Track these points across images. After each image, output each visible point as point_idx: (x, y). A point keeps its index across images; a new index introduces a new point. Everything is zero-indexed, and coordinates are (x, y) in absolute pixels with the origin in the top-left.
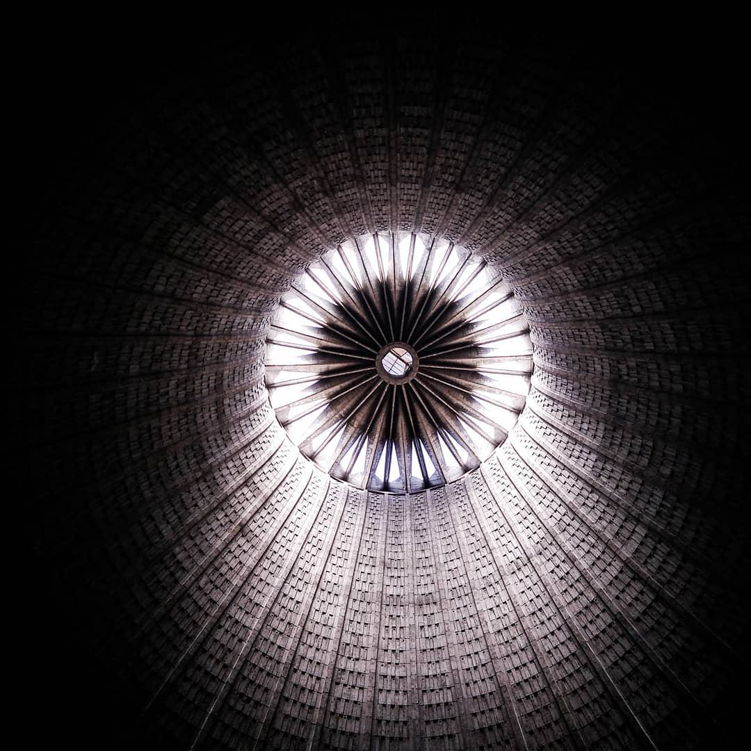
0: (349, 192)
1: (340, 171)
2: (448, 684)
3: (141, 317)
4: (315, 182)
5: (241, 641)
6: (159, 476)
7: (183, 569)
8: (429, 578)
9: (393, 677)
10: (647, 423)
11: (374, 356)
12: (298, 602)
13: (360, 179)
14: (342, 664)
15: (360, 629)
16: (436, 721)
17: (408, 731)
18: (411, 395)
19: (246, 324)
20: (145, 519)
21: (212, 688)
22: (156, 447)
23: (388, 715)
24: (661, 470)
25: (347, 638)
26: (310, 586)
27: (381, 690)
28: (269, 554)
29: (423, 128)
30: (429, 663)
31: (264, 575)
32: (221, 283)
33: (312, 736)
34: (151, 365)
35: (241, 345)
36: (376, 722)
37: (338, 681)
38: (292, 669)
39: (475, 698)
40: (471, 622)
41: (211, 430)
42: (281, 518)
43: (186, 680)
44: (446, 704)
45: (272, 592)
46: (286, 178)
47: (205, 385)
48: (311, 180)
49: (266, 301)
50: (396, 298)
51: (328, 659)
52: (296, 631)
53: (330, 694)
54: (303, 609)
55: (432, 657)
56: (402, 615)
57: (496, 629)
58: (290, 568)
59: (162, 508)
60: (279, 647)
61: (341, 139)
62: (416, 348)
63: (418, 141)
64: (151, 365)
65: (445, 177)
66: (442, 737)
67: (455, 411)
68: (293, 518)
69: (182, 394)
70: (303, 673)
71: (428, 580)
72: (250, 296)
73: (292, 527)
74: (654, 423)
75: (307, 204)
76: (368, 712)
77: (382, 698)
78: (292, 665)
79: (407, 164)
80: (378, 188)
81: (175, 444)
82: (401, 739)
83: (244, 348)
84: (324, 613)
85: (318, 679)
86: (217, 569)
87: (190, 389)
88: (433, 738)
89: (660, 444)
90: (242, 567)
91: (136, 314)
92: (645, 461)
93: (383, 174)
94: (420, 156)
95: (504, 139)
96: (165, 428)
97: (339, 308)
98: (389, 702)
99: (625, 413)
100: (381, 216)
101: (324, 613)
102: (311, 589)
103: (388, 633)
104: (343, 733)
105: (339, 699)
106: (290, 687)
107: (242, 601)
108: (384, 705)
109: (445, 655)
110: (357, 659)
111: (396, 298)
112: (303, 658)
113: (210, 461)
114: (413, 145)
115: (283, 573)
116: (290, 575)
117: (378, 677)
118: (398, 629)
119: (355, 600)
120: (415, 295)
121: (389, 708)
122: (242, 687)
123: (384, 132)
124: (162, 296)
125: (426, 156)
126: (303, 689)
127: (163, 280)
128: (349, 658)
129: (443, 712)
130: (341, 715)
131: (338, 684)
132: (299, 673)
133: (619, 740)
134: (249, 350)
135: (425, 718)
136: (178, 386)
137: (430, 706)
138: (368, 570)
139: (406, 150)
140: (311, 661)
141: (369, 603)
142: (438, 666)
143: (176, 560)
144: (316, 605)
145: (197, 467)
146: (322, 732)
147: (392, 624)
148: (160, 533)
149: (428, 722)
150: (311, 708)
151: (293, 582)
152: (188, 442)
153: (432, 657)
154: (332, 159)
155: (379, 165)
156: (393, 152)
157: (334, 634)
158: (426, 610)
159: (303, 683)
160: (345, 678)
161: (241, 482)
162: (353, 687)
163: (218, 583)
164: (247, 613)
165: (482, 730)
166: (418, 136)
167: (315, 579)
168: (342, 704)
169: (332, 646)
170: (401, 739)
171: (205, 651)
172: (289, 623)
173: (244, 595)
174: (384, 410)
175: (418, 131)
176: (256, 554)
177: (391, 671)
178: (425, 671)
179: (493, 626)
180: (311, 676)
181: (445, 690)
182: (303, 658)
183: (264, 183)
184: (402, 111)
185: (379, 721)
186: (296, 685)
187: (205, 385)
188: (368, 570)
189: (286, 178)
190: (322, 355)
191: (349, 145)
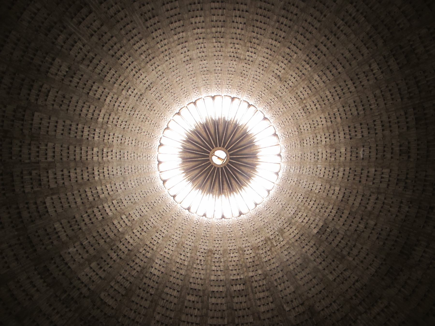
0: (258, 240)
1: (265, 251)
2: (173, 31)
4: (275, 245)
8: (189, 70)
10: (108, 167)
11: (230, 155)
13: (256, 248)
16: (176, 15)
18: (210, 144)
19: (293, 169)
20: (327, 82)
24: (98, 149)
29: (233, 280)
30: (183, 38)
32: (309, 190)
35: (294, 159)
39: (159, 29)
41: (302, 121)
44: (172, 23)
46: (289, 246)
47: (308, 142)
48: (277, 245)
49: (286, 180)
55: (181, 40)
56: (199, 54)
57: (155, 59)
59: (320, 87)
60: (254, 32)
61: (268, 268)
62: (212, 166)
63: (234, 272)
65: (218, 256)
66: (171, 9)
71: (188, 70)
72: (294, 184)
74: (105, 168)
75: (276, 232)
77: (202, 19)
79: (236, 259)
80: (246, 244)
82: (190, 4)
83: (292, 158)
87: (315, 141)
88: (175, 8)
89: (100, 160)
91: (346, 176)
92: (105, 150)
93: (245, 252)
94: (231, 264)
95: (198, 282)
96: (324, 122)
98: (199, 18)
99: (118, 168)
100: (241, 229)
103: (204, 45)
109: (177, 42)
113: (300, 107)
114: (236, 270)
118: (199, 48)
120: (217, 189)
123: (251, 274)
125: (229, 265)
127: (336, 193)
129: (173, 20)
133: (92, 30)
134: (290, 156)
135: (181, 15)
137: (179, 21)
138: (217, 68)
139: (238, 267)
142: (179, 37)
143: (309, 65)
145: (306, 105)
147: (203, 50)
149: (179, 14)
152: (312, 116)
153: (181, 40)
154: (270, 257)
155: (248, 257)
156: (244, 265)
158: (188, 58)
165: (154, 17)
166: (234, 275)
175: (235, 278)
177: (199, 31)
178: (184, 34)
179: (156, 60)
181: (173, 28)
183: (298, 242)
184: (244, 286)
187: (308, 142)
188: (217, 68)
189: (289, 246)
191: (264, 265)
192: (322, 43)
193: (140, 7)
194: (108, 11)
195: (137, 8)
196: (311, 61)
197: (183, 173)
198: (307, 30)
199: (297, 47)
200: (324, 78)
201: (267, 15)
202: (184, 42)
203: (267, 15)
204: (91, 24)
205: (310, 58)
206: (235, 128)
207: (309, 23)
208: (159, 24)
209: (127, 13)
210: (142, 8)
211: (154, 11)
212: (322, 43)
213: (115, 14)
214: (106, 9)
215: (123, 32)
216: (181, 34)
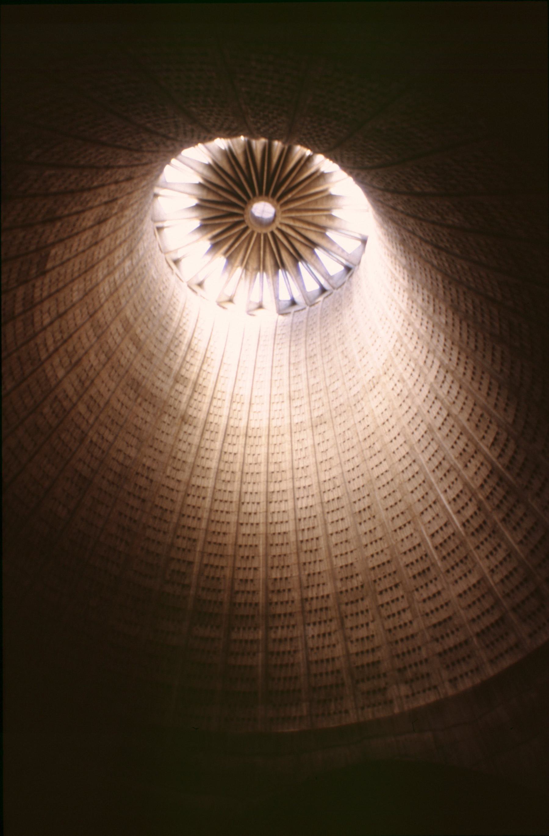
3: (46, 345)
5: (204, 498)
6: (113, 420)
7: (153, 470)
9: (304, 487)
12: (235, 454)
14: (271, 488)
15: (279, 458)
17: (317, 521)
21: (195, 535)
22: (102, 405)
23: (304, 514)
25: (272, 468)
26: (241, 437)
27: (298, 499)
28: (208, 427)
30: (325, 471)
31: (207, 446)
33: (261, 542)
34: (71, 362)
36: (298, 521)
37: (271, 501)
38: (241, 503)
40: (348, 434)
42: (209, 392)
43: (178, 537)
45: (216, 455)
50: (241, 159)
51: (261, 488)
52: (238, 476)
53: (267, 512)
54: (239, 458)
58: (224, 431)
62: (273, 195)
64: (71, 362)
67: (322, 229)
68: (219, 387)
69: (103, 357)
70: (248, 503)
73: (219, 396)
76: (292, 516)
77: (299, 504)
78: (240, 500)
81: (114, 392)
84: (254, 455)
85: (258, 503)
86: (175, 458)
87: (106, 349)
90: (191, 447)
91: (41, 347)
97: (209, 166)
101: (254, 455)
102: (242, 440)
104: (279, 534)
105: (273, 513)
106: (242, 515)
107: (198, 471)
108: (301, 508)
110: (281, 481)
111: (241, 159)
112: (246, 493)
115: (220, 437)
116: (226, 435)
117: (295, 489)
119: (273, 436)
121: (304, 509)
122: (213, 528)
124: (51, 323)
126: (250, 514)
128: (276, 482)
130: (276, 523)
131: (271, 502)
132: (245, 504)
136: (96, 355)
140: (251, 493)
141: (283, 435)
144: (248, 451)
146: (267, 537)
148: (130, 457)
150: (257, 524)
151: (229, 440)
157: (263, 468)
159: (249, 510)
160: (275, 497)
161: (186, 349)
162: (281, 501)
163: (179, 467)
164: (203, 477)
167: (243, 431)
168: (275, 515)
169: (263, 478)
170: (314, 528)
171: (183, 515)
172: (233, 472)
173: (198, 466)
174: (268, 250)
176: (198, 432)
180: (253, 503)
182: (246, 493)
185: (300, 520)
186: (245, 513)
190: (204, 227)
192: (137, 509)
193: (375, 529)
194: (412, 531)
195: (379, 529)
196: (146, 474)
197: (262, 277)
198: (160, 519)
199: (168, 487)
200: (121, 458)
201: (216, 525)
202: (324, 461)
203: (216, 525)
204: (434, 519)
205: (147, 478)
206: (247, 263)
207: (159, 531)
208: (354, 500)
209: (390, 523)
210: (372, 528)
211: (359, 520)
212: (137, 509)
213: (405, 525)
214: (415, 535)
215: (398, 496)
216: (327, 478)
